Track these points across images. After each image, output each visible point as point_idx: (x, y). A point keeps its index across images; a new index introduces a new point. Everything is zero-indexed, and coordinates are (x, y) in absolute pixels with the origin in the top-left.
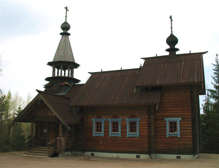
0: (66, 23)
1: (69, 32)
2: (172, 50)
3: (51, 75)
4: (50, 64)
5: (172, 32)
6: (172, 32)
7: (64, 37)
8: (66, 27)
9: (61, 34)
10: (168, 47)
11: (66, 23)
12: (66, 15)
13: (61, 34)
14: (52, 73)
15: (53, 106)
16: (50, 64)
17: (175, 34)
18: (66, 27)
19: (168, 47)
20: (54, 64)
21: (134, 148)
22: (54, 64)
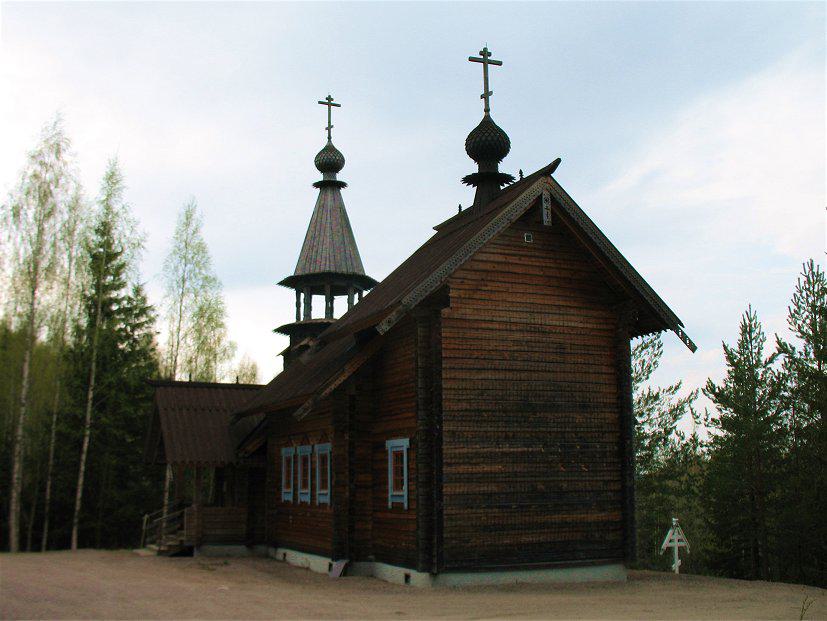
0: (330, 148)
1: (340, 177)
2: (487, 180)
3: (290, 319)
4: (288, 282)
5: (487, 110)
6: (487, 110)
7: (330, 194)
8: (330, 162)
9: (316, 185)
10: (473, 168)
11: (330, 148)
12: (329, 122)
13: (316, 185)
14: (313, 304)
15: (465, 320)
16: (288, 282)
17: (499, 120)
18: (330, 162)
19: (473, 168)
20: (303, 283)
21: (535, 349)
22: (303, 283)
